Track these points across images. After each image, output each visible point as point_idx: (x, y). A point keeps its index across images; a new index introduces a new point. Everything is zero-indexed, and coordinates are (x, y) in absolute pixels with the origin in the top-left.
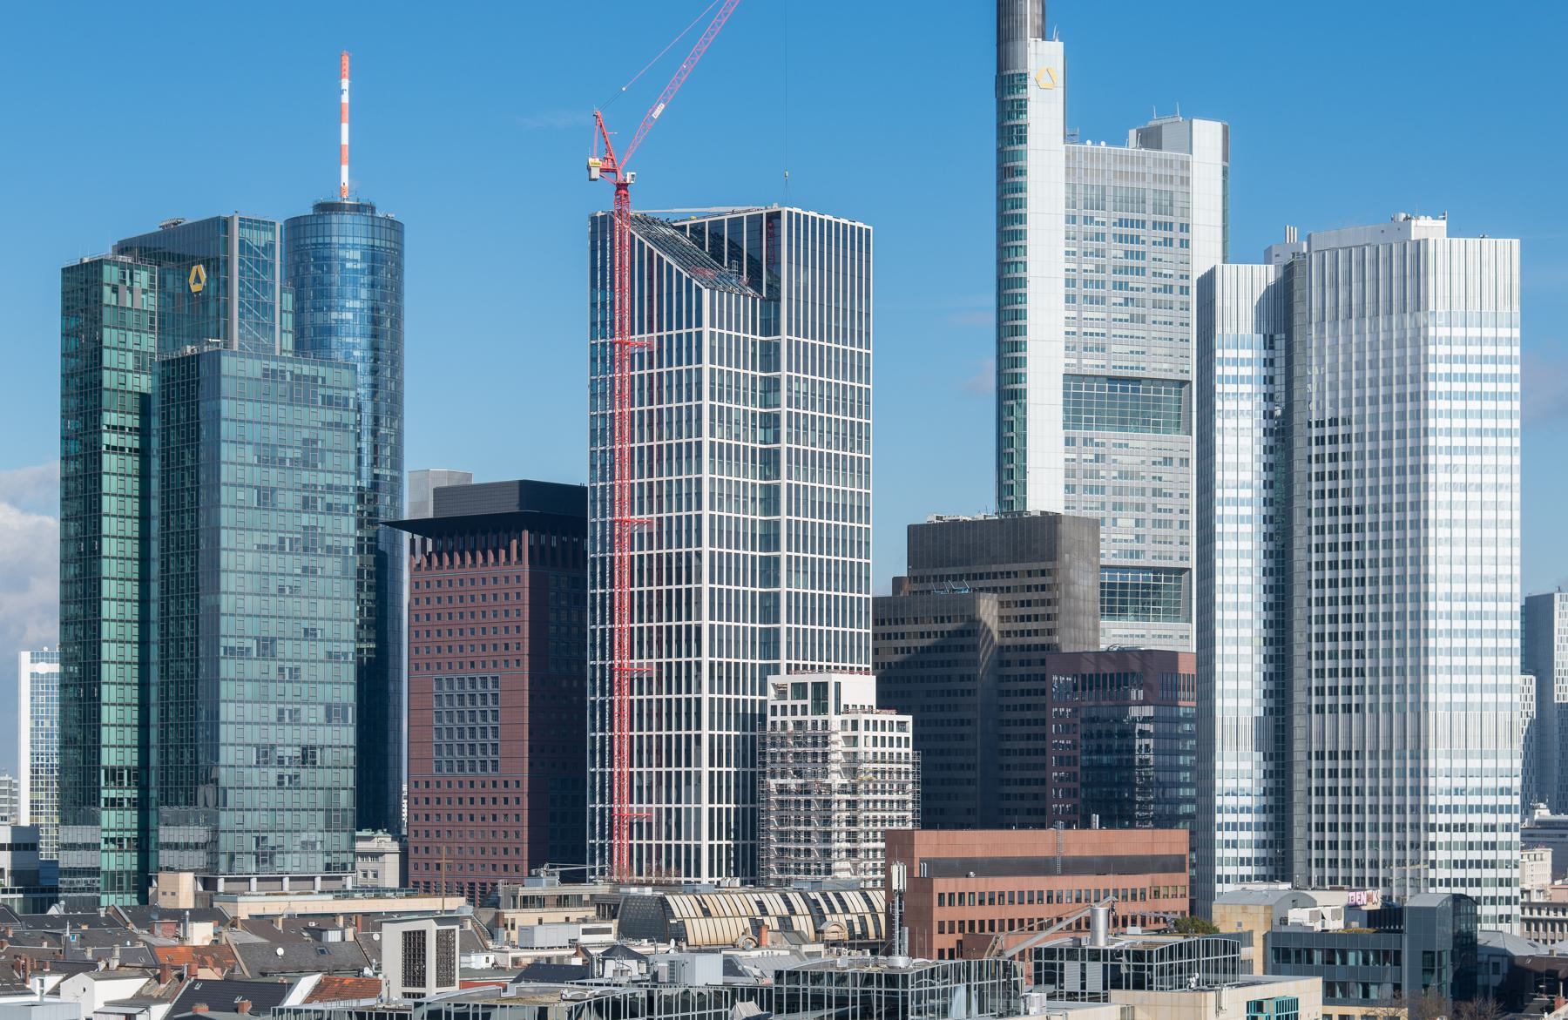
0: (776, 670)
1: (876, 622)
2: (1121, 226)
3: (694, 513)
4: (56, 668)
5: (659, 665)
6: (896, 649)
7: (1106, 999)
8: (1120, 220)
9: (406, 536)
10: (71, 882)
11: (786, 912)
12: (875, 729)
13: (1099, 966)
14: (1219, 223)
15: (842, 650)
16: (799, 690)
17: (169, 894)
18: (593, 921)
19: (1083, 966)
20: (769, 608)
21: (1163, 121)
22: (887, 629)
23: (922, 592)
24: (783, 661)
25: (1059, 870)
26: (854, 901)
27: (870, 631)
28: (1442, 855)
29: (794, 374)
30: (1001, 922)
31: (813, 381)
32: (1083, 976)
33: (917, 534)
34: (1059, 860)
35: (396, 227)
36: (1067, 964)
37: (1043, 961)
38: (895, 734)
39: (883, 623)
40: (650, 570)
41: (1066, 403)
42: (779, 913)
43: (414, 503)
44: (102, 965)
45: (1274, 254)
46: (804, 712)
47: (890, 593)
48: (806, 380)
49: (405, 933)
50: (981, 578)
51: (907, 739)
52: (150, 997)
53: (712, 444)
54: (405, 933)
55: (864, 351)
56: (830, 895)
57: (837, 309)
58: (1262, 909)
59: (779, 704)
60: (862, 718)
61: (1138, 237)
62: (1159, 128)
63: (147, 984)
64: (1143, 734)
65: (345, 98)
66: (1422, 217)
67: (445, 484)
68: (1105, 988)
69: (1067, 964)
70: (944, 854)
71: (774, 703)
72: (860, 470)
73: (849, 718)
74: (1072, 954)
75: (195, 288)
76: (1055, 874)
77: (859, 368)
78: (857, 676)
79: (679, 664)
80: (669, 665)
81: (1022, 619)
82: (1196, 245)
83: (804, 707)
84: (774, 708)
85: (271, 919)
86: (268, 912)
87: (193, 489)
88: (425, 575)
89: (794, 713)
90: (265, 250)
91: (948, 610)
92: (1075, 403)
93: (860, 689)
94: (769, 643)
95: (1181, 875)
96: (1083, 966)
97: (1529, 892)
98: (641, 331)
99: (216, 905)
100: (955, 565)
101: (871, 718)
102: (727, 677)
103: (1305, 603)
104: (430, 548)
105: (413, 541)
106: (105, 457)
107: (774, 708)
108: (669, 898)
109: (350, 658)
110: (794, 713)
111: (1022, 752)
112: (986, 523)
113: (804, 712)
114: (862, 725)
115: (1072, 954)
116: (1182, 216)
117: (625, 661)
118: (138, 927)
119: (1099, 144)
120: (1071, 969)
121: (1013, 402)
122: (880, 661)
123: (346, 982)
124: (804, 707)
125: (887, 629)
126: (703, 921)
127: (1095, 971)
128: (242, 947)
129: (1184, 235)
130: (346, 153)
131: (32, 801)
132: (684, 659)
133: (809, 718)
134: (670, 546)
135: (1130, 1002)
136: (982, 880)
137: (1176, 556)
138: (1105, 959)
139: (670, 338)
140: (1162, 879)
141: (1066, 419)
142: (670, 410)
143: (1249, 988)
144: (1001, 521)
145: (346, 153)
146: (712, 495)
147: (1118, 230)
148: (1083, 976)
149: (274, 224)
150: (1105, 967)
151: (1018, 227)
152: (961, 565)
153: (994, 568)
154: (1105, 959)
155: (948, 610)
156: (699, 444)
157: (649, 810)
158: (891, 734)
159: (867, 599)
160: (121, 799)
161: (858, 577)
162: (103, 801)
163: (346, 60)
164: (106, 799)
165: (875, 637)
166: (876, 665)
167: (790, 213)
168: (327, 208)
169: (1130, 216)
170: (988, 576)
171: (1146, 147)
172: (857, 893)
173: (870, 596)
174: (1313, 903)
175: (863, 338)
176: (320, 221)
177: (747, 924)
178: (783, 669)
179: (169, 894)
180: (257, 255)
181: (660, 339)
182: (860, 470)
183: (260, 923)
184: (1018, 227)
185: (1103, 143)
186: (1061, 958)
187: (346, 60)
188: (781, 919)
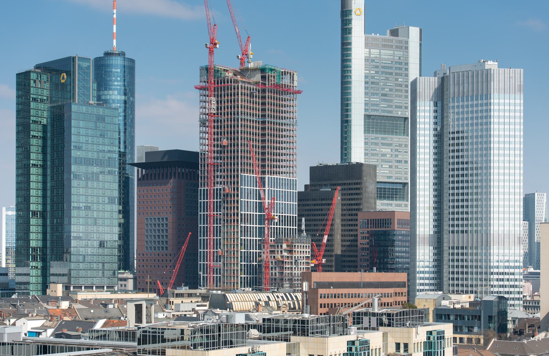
4: (14, 213)
9: (136, 168)
11: (267, 300)
13: (375, 318)
17: (54, 291)
18: (200, 302)
19: (370, 319)
23: (315, 190)
27: (297, 203)
32: (370, 322)
33: (313, 170)
34: (362, 283)
35: (132, 61)
36: (364, 317)
39: (301, 201)
42: (265, 300)
43: (138, 157)
44: (30, 315)
45: (437, 73)
66: (489, 61)
69: (364, 317)
75: (63, 81)
81: (350, 200)
103: (448, 195)
104: (144, 173)
105: (138, 170)
108: (227, 294)
115: (366, 314)
117: (212, 213)
118: (43, 303)
119: (377, 35)
120: (366, 319)
123: (115, 322)
127: (374, 320)
140: (398, 290)
141: (365, 131)
148: (370, 322)
150: (377, 319)
159: (296, 192)
161: (292, 184)
162: (31, 99)
165: (299, 205)
171: (393, 36)
173: (297, 191)
179: (54, 291)
184: (349, 58)
185: (378, 35)
188: (266, 302)
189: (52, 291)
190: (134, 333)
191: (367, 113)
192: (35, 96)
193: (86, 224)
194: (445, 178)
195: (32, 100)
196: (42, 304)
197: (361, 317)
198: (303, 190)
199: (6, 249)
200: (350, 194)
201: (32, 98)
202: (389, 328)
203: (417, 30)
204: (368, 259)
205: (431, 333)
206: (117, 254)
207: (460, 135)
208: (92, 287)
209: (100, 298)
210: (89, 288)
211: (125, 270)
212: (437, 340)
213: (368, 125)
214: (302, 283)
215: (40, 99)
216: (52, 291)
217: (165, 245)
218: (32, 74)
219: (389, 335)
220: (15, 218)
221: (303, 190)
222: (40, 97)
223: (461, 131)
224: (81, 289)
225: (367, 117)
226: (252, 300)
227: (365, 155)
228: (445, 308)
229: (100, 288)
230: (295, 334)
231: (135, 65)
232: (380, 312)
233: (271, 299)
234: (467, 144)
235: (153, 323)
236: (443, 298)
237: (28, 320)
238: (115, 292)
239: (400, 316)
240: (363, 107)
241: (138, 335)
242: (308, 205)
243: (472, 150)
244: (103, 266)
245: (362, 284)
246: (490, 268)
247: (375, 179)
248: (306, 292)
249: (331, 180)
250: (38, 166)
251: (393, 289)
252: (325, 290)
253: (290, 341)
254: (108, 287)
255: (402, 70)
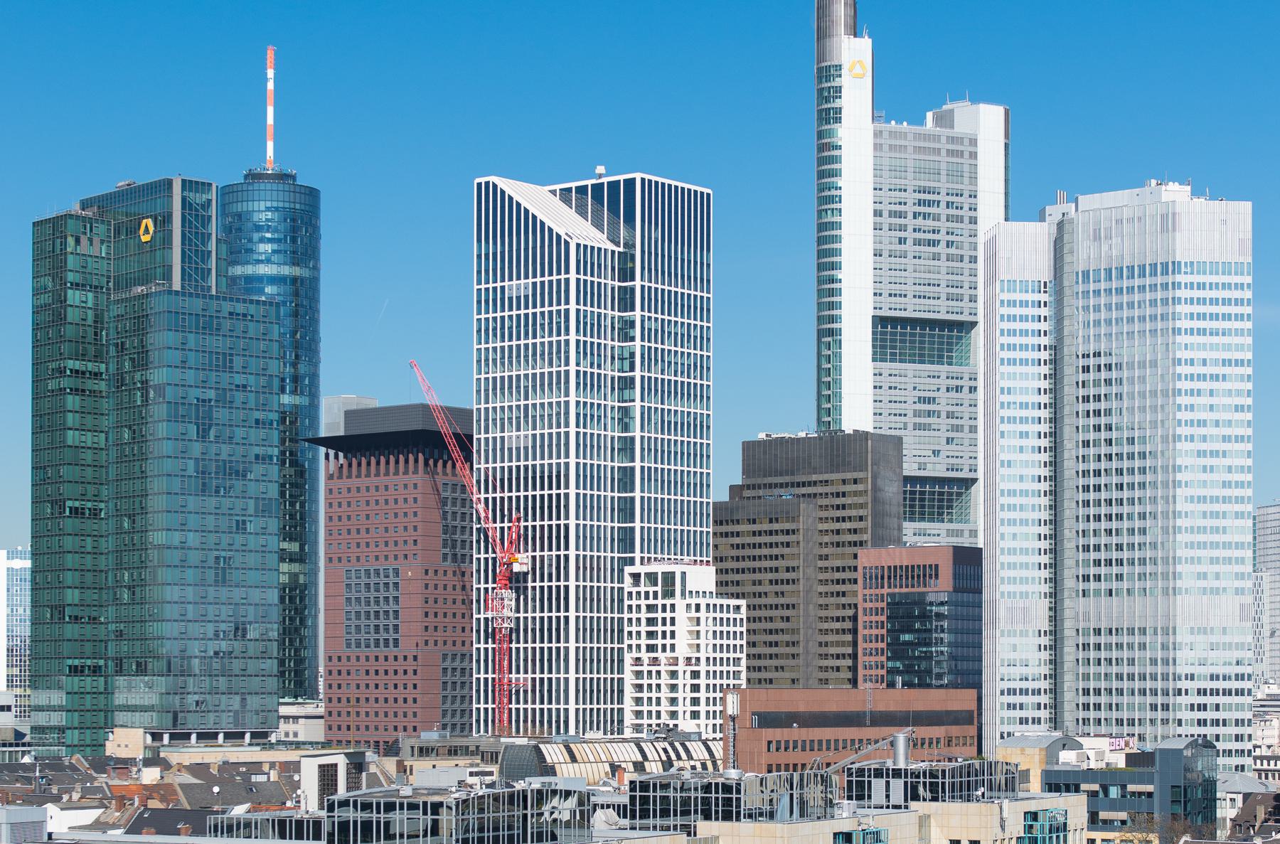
0: (631, 562)
1: (715, 522)
2: (920, 205)
3: (562, 553)
4: (28, 564)
5: (534, 680)
6: (732, 545)
7: (906, 807)
8: (920, 200)
9: (322, 450)
10: (40, 738)
11: (640, 758)
12: (715, 611)
13: (900, 782)
14: (1002, 140)
15: (684, 545)
16: (652, 578)
17: (123, 746)
18: (477, 765)
19: (888, 783)
20: (626, 510)
21: (955, 105)
22: (724, 528)
23: (754, 498)
24: (637, 555)
25: (868, 722)
26: (698, 751)
28: (1182, 309)
29: (646, 314)
30: (820, 742)
31: (663, 320)
32: (888, 796)
33: (752, 451)
34: (868, 714)
35: (313, 194)
36: (873, 780)
37: (854, 779)
38: (732, 616)
39: (721, 524)
40: (526, 479)
41: (874, 340)
42: (634, 759)
43: (330, 422)
44: (65, 797)
46: (655, 597)
47: (727, 499)
48: (656, 319)
49: (320, 766)
50: (804, 486)
51: (742, 620)
52: (107, 823)
53: (578, 372)
54: (320, 766)
55: (705, 295)
56: (677, 745)
57: (683, 260)
58: (1037, 751)
59: (634, 590)
60: (703, 602)
61: (934, 399)
62: (952, 111)
63: (104, 813)
64: (939, 616)
65: (270, 85)
66: (1171, 183)
67: (354, 407)
68: (906, 800)
69: (873, 780)
70: (771, 708)
71: (630, 590)
72: (702, 309)
73: (694, 601)
74: (878, 773)
75: (145, 238)
76: (865, 726)
77: (702, 309)
78: (698, 567)
79: (550, 588)
80: (542, 527)
81: (838, 520)
82: (981, 214)
83: (655, 593)
84: (630, 594)
85: (207, 766)
86: (206, 761)
87: (143, 388)
88: (336, 483)
89: (647, 597)
90: (203, 206)
91: (776, 513)
92: (882, 340)
93: (703, 577)
94: (626, 540)
95: (971, 727)
96: (888, 783)
97: (1260, 747)
98: (519, 278)
99: (162, 755)
100: (781, 475)
101: (712, 601)
102: (588, 568)
103: (1074, 504)
106: (70, 292)
107: (630, 594)
108: (542, 746)
109: (275, 461)
110: (647, 597)
111: (837, 631)
112: (806, 440)
113: (655, 597)
114: (703, 608)
115: (878, 773)
116: (971, 184)
118: (96, 772)
119: (902, 123)
120: (878, 785)
121: (830, 339)
122: (718, 555)
124: (655, 593)
125: (724, 528)
126: (570, 766)
127: (898, 785)
128: (184, 787)
129: (972, 214)
130: (270, 131)
131: (8, 676)
132: (554, 522)
133: (660, 602)
134: (542, 458)
135: (927, 812)
136: (804, 730)
137: (966, 312)
138: (906, 777)
139: (542, 283)
140: (955, 730)
141: (874, 353)
142: (542, 344)
143: (1026, 802)
144: (820, 438)
145: (270, 131)
146: (578, 415)
147: (918, 209)
148: (888, 796)
149: (210, 185)
150: (906, 783)
151: (835, 246)
152: (787, 475)
153: (814, 477)
154: (906, 777)
155: (776, 513)
156: (567, 372)
157: (526, 679)
158: (728, 616)
159: (708, 503)
160: (83, 509)
161: (702, 486)
162: (68, 510)
163: (270, 55)
164: (71, 508)
165: (715, 534)
166: (715, 559)
167: (643, 180)
168: (253, 177)
169: (927, 184)
170: (810, 484)
171: (941, 127)
172: (700, 743)
173: (711, 501)
174: (1080, 746)
175: (705, 283)
176: (251, 188)
177: (608, 768)
178: (638, 561)
179: (123, 746)
180: (197, 210)
181: (534, 284)
182: (699, 394)
183: (199, 769)
184: (835, 246)
185: (905, 123)
186: (869, 776)
187: (270, 55)
188: (635, 764)
189: (119, 746)
190: (317, 824)
191: (879, 313)
192: (77, 504)
193: (202, 583)
194: (1066, 463)
195: (71, 513)
196: (95, 775)
197: (866, 779)
198: (725, 497)
199: (8, 650)
200: (838, 507)
201: (71, 508)
202: (934, 804)
203: (999, 111)
204: (882, 649)
205: (1034, 816)
206: (275, 654)
207: (1103, 361)
208: (215, 736)
209: (235, 760)
210: (207, 737)
211: (296, 697)
212: (1050, 832)
213: (882, 340)
214: (725, 695)
215: (90, 509)
216: (119, 746)
217: (392, 621)
218: (70, 222)
219: (932, 820)
220: (29, 577)
221: (725, 497)
222: (89, 505)
223: (1105, 353)
224: (189, 739)
225: (880, 322)
226: (604, 759)
227: (875, 149)
228: (1069, 768)
229: (234, 736)
230: (707, 816)
231: (319, 274)
232: (913, 767)
233: (650, 757)
234: (1120, 382)
235: (364, 790)
236: (1064, 745)
237: (62, 809)
238: (271, 746)
239: (961, 777)
240: (869, 301)
241: (325, 829)
242: (738, 534)
243: (1131, 396)
244: (244, 700)
245: (868, 718)
246: (1174, 471)
247: (898, 470)
248: (733, 719)
249: (793, 474)
250: (83, 514)
251: (943, 728)
252: (778, 731)
253: (695, 835)
254: (254, 735)
255: (962, 536)
